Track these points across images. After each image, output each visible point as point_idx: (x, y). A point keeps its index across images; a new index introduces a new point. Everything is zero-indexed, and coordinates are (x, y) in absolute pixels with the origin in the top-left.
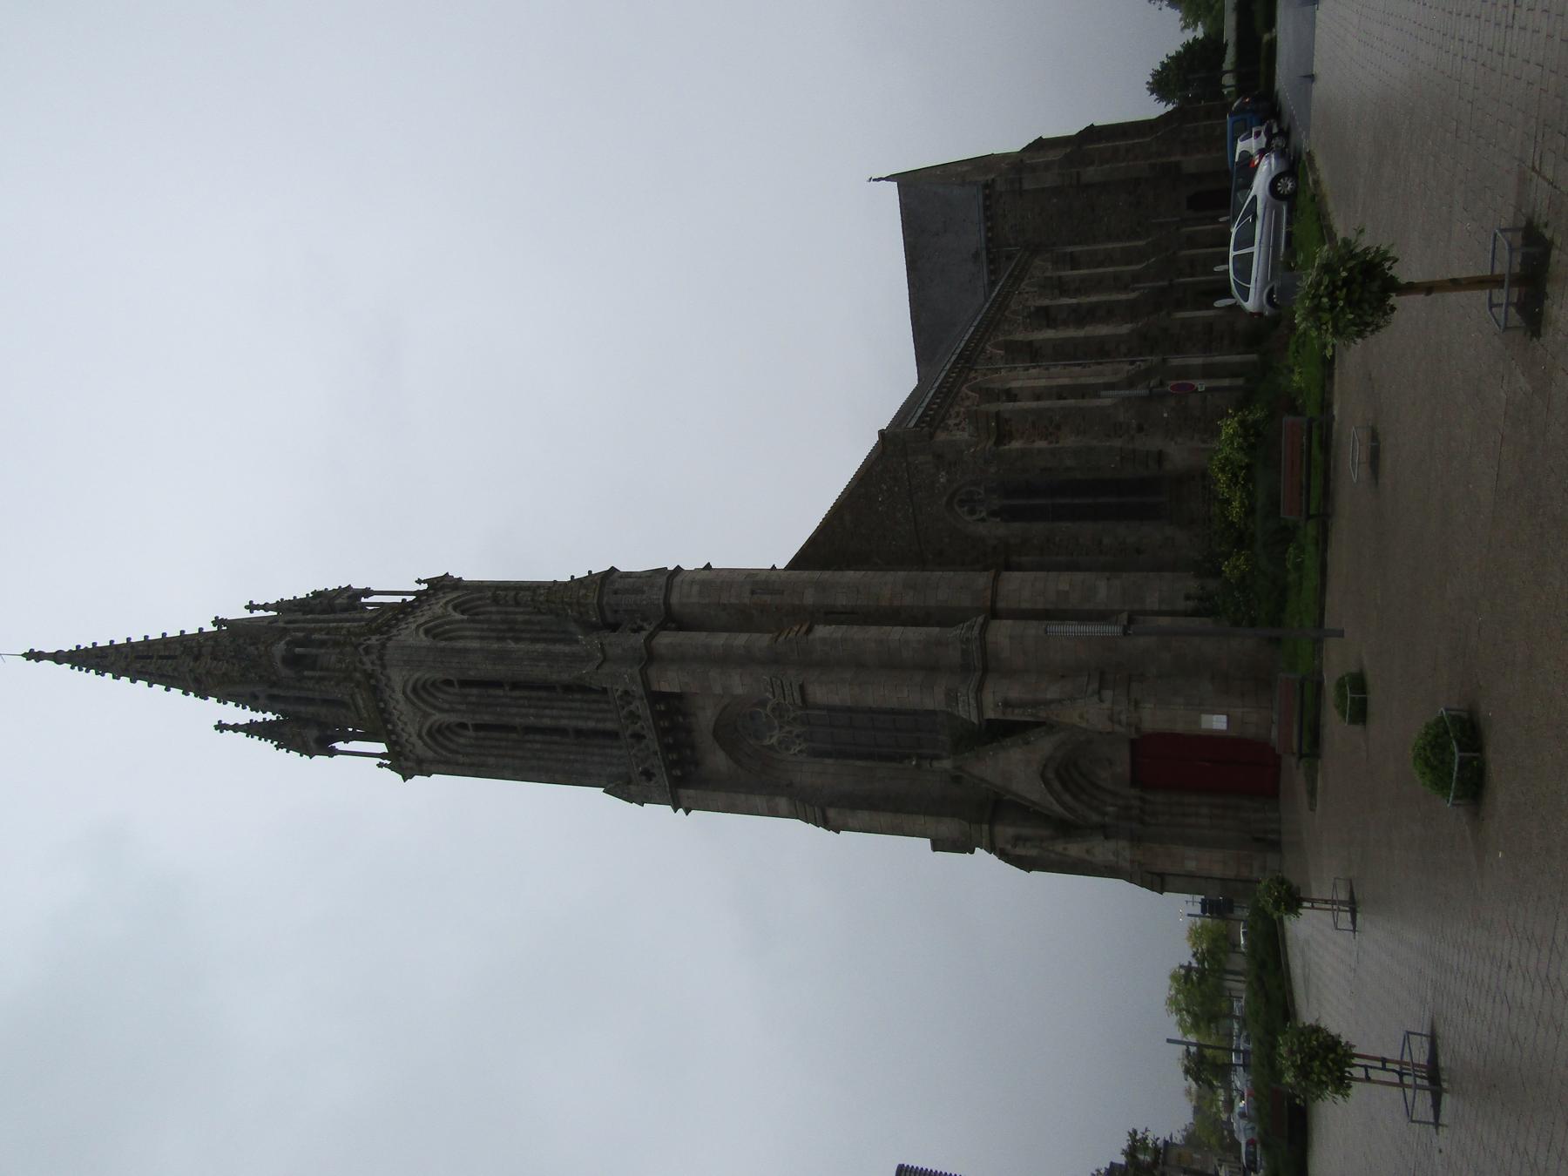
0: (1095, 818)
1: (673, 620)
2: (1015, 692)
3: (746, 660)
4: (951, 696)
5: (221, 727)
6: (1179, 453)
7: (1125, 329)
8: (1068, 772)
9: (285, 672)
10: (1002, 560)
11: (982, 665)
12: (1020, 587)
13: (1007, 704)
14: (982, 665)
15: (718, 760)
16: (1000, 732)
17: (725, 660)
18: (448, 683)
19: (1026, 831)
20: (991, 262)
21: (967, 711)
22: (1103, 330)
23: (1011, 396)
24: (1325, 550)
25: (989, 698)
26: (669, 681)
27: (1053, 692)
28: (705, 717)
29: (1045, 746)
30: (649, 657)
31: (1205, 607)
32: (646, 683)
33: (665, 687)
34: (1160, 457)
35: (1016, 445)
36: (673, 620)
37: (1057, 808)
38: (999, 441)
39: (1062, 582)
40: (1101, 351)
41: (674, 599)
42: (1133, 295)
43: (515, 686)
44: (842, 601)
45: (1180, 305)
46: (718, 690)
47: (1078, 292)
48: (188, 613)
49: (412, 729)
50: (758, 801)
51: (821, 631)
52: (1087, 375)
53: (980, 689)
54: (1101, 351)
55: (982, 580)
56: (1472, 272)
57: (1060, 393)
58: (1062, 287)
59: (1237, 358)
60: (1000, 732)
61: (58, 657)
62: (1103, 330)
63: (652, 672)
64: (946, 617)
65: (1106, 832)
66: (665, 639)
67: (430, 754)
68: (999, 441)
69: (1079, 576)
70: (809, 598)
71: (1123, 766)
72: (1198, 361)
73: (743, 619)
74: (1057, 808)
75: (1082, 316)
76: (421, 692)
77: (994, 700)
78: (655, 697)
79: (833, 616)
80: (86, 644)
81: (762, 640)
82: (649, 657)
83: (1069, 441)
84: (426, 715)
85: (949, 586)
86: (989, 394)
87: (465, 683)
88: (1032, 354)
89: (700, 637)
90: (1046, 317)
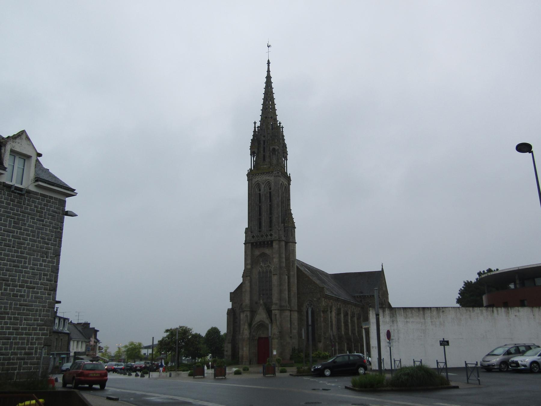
0: (252, 331)
1: (287, 243)
2: (278, 316)
3: (280, 262)
4: (276, 304)
5: (255, 123)
6: (321, 345)
7: (343, 333)
8: (262, 326)
9: (271, 148)
10: (300, 311)
11: (282, 309)
12: (295, 315)
13: (276, 315)
14: (282, 309)
15: (257, 253)
16: (269, 312)
17: (280, 257)
18: (270, 189)
19: (249, 317)
20: (360, 296)
21: (273, 307)
22: (343, 328)
23: (331, 312)
24: (430, 308)
25: (277, 312)
26: (275, 245)
27: (278, 323)
28: (267, 251)
29: (267, 321)
30: (280, 241)
31: (294, 350)
32: (275, 240)
33: (274, 244)
34: (320, 342)
35: (322, 314)
36: (287, 243)
37: (254, 324)
38: (323, 311)
39: (296, 324)
40: (339, 328)
41: (291, 244)
42: (350, 334)
43: (270, 205)
44: (292, 280)
45: (348, 344)
46: (274, 256)
47: (351, 320)
48: (282, 117)
49: (259, 179)
50: (249, 262)
51: (287, 277)
52: (334, 327)
53: (278, 310)
54: (339, 328)
55: (296, 308)
56: (303, 205)
57: (331, 322)
58: (352, 317)
59: (263, 387)
60: (269, 312)
61: (268, 71)
62: (343, 328)
63: (277, 242)
64: (290, 302)
65: (250, 333)
66: (283, 243)
67: (253, 183)
68: (323, 311)
69: (297, 327)
70: (292, 273)
71: (262, 336)
72: (337, 348)
73: (287, 259)
74: (254, 324)
75: (346, 325)
76: (269, 183)
77: (275, 312)
78: (272, 242)
79: (289, 278)
80: (272, 80)
81: (284, 265)
82: (280, 241)
83: (323, 324)
84: (263, 184)
85: (294, 301)
86: (331, 308)
87: (270, 193)
88: (338, 314)
89: (284, 252)
90: (346, 315)
